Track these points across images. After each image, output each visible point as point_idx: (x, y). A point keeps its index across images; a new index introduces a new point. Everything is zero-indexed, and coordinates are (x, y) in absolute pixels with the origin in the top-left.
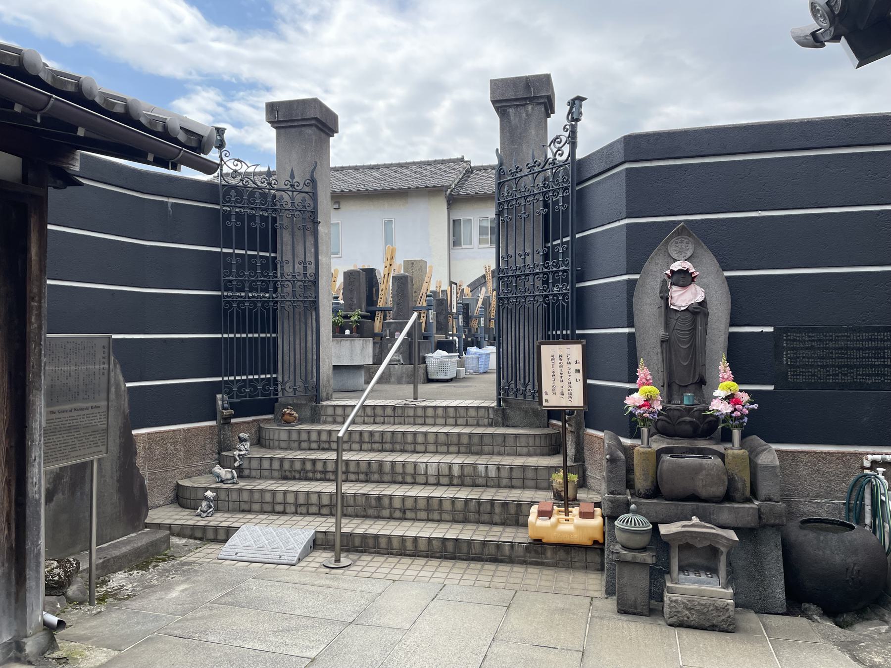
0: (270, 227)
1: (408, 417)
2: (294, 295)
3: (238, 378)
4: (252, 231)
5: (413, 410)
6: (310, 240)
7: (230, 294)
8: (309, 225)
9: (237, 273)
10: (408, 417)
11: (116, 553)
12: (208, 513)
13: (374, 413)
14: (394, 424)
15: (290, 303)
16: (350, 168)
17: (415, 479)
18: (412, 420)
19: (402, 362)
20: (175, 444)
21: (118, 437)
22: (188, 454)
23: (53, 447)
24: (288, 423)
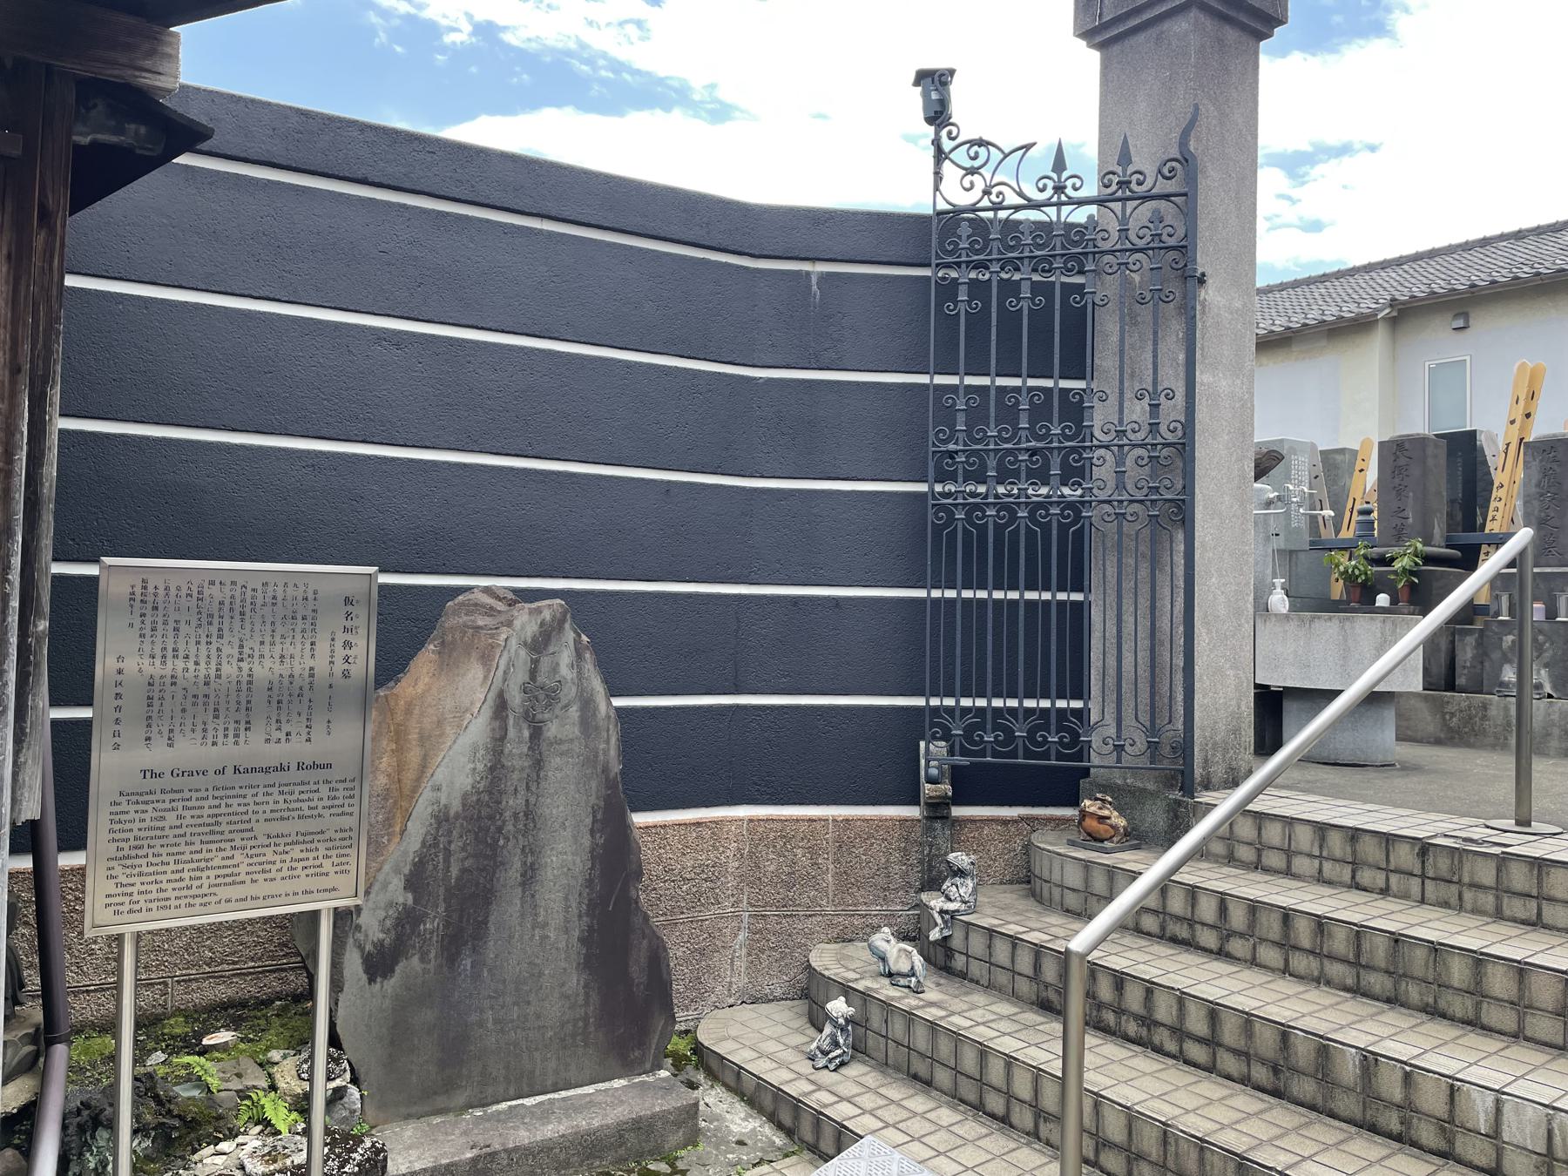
0: (1057, 306)
1: (1475, 886)
2: (1120, 486)
3: (966, 702)
4: (1010, 321)
5: (1492, 865)
6: (1174, 332)
7: (951, 488)
8: (1174, 287)
9: (968, 432)
10: (1475, 886)
11: (523, 1136)
12: (830, 1061)
13: (1354, 852)
14: (1423, 901)
15: (1107, 508)
16: (1503, 237)
17: (1451, 1142)
18: (1488, 900)
19: (1548, 689)
20: (813, 851)
21: (585, 831)
22: (845, 881)
23: (151, 869)
24: (1094, 839)
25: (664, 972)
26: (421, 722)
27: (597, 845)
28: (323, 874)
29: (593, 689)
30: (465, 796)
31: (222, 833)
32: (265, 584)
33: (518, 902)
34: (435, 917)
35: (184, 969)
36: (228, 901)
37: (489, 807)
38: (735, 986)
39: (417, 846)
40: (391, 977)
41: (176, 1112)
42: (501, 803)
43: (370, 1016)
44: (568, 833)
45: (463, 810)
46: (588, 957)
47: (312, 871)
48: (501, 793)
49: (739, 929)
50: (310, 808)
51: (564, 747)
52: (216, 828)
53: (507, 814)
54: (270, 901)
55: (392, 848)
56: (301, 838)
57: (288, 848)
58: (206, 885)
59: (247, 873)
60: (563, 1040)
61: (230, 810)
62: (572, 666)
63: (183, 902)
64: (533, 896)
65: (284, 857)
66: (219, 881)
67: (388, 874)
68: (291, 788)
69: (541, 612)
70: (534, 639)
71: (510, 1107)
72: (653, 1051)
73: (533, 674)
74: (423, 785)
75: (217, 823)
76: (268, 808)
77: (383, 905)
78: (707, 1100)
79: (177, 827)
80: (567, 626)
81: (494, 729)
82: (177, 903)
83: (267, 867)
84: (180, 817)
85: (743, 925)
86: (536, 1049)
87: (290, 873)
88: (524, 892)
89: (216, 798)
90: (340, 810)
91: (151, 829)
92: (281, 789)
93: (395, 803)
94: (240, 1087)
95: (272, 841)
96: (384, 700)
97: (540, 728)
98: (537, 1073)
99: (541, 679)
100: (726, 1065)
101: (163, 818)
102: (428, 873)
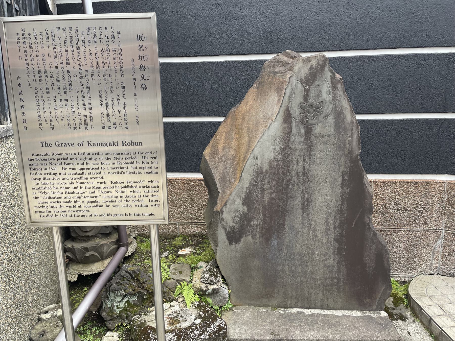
21: (338, 185)
23: (54, 195)
25: (385, 262)
26: (248, 124)
27: (345, 193)
28: (144, 205)
29: (342, 106)
30: (270, 162)
31: (87, 179)
32: (88, 28)
33: (300, 217)
34: (258, 219)
35: (182, 220)
36: (96, 215)
37: (283, 168)
38: (434, 266)
39: (248, 185)
40: (239, 243)
41: (146, 288)
42: (290, 167)
43: (231, 259)
44: (328, 185)
45: (270, 169)
46: (339, 249)
47: (138, 203)
48: (289, 162)
49: (438, 238)
50: (133, 168)
51: (325, 139)
52: (84, 176)
53: (293, 173)
54: (117, 218)
55: (236, 184)
56: (130, 185)
57: (123, 190)
58: (83, 206)
59: (103, 202)
60: (326, 286)
61: (89, 166)
62: (330, 93)
63: (73, 214)
64: (308, 215)
65: (122, 194)
66: (89, 204)
67: (234, 197)
68: (121, 155)
69: (310, 61)
70: (306, 77)
71: (298, 312)
72: (377, 301)
73: (306, 97)
74: (249, 156)
75: (83, 173)
76: (109, 166)
77: (233, 210)
78: (409, 330)
79: (64, 174)
80: (326, 69)
81: (284, 128)
82: (70, 214)
83: (114, 199)
84: (63, 169)
85: (441, 237)
86: (312, 288)
87: (126, 203)
88: (303, 212)
89: (81, 159)
90: (150, 170)
91: (50, 174)
92: (115, 156)
93: (237, 163)
94: (179, 279)
95: (114, 185)
96: (234, 113)
97: (311, 128)
98: (312, 299)
99: (311, 101)
100: (423, 313)
101: (55, 169)
102: (254, 198)
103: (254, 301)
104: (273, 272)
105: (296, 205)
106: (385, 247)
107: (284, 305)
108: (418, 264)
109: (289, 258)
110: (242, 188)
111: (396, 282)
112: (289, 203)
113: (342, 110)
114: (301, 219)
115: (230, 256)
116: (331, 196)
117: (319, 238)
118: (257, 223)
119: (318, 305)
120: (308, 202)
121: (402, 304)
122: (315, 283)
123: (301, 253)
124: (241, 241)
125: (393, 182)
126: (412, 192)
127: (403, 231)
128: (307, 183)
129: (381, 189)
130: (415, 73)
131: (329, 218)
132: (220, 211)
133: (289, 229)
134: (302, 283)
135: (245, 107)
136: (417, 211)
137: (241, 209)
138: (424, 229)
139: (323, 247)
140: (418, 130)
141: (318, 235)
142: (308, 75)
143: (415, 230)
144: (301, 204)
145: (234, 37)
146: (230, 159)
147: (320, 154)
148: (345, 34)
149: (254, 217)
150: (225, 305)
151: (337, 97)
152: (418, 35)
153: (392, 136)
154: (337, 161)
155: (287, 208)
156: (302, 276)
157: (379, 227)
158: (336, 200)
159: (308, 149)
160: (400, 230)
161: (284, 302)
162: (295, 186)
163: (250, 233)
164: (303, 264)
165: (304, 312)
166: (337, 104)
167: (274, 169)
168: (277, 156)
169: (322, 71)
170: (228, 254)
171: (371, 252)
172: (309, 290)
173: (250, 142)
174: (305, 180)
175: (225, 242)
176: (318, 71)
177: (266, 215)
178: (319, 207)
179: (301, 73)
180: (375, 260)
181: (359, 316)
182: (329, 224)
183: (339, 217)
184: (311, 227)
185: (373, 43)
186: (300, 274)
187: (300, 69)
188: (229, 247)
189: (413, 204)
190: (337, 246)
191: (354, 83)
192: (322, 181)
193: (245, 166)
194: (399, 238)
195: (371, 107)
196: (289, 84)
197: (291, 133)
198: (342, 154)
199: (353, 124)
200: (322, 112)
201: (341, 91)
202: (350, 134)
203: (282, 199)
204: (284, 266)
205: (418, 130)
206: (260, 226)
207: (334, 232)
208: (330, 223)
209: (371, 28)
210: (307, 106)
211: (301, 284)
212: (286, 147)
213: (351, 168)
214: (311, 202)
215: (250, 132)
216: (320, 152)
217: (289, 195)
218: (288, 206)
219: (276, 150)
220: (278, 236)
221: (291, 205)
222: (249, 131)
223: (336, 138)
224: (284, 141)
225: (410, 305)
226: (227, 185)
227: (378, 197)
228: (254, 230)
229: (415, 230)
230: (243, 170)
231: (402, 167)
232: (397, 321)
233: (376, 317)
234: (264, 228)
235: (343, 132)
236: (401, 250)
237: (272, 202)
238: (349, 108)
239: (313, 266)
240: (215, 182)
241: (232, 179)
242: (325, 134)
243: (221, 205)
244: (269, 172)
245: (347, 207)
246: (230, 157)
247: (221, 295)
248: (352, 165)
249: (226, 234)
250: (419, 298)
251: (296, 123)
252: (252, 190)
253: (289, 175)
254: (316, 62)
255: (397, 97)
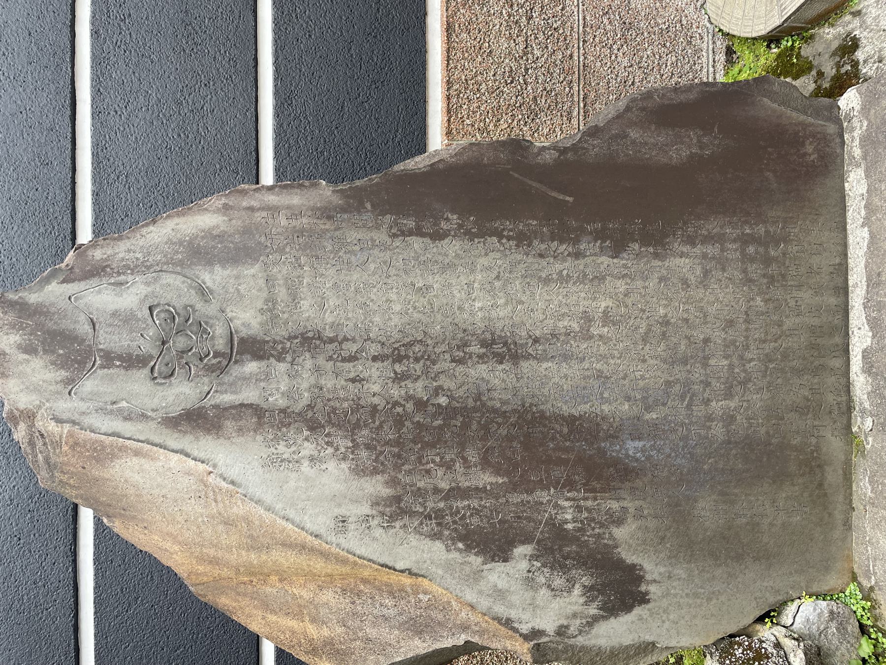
21: (435, 249)
25: (683, 97)
27: (460, 226)
29: (170, 242)
30: (359, 471)
33: (545, 365)
34: (556, 506)
37: (381, 426)
39: (438, 545)
40: (642, 569)
42: (376, 406)
43: (696, 595)
44: (436, 281)
45: (383, 472)
46: (647, 239)
51: (282, 293)
53: (396, 392)
60: (772, 280)
64: (536, 341)
70: (63, 363)
72: (810, 120)
74: (334, 550)
77: (529, 594)
80: (33, 298)
88: (528, 357)
97: (242, 341)
98: (816, 322)
99: (147, 346)
103: (836, 512)
104: (734, 452)
105: (504, 381)
106: (633, 100)
107: (843, 413)
108: (676, 16)
109: (682, 398)
110: (448, 567)
111: (730, 75)
112: (498, 405)
113: (181, 243)
114: (550, 364)
115: (687, 600)
116: (472, 271)
117: (611, 304)
118: (571, 511)
119: (835, 303)
120: (494, 342)
121: (799, 52)
122: (763, 314)
123: (665, 361)
124: (635, 562)
125: (448, 89)
126: (475, 39)
127: (585, 58)
128: (430, 348)
129: (468, 119)
130: (143, 36)
131: (544, 276)
132: (532, 643)
133: (586, 403)
134: (767, 355)
135: (174, 556)
136: (528, 23)
137: (524, 565)
138: (578, 5)
139: (642, 290)
140: (304, 25)
141: (603, 306)
142: (53, 358)
143: (581, 28)
144: (501, 363)
145: (22, 541)
146: (353, 603)
147: (332, 307)
148: (27, 225)
149: (551, 523)
150: (855, 612)
151: (137, 259)
152: (38, 30)
153: (320, 94)
154: (356, 255)
155: (515, 411)
156: (741, 358)
157: (575, 122)
158: (486, 254)
159: (316, 347)
160: (582, 68)
161: (830, 412)
162: (440, 387)
163: (604, 533)
164: (700, 354)
165: (864, 351)
166: (159, 258)
167: (382, 458)
168: (337, 449)
169: (41, 313)
170: (680, 607)
171: (652, 140)
172: (788, 333)
173: (287, 545)
174: (419, 355)
175: (641, 618)
176: (39, 326)
177: (541, 480)
178: (510, 308)
179: (44, 381)
180: (677, 129)
181: (867, 177)
182: (565, 272)
183: (542, 241)
184: (578, 329)
185: (56, 149)
186: (735, 360)
187: (27, 388)
188: (657, 604)
189: (510, 33)
190: (636, 246)
191: (168, 198)
192: (422, 299)
193: (370, 560)
194: (606, 69)
195: (238, 151)
196: (78, 424)
197: (258, 405)
198: (332, 238)
199: (231, 208)
200: (185, 307)
201: (115, 247)
202: (264, 214)
203: (485, 428)
204: (711, 415)
205: (304, 25)
206: (579, 500)
207: (592, 258)
208: (562, 271)
209: (14, 156)
210: (164, 358)
211: (768, 359)
212: (306, 421)
213: (381, 209)
214: (493, 334)
215: (255, 544)
216: (326, 310)
217: (470, 403)
218: (510, 408)
219: (316, 453)
220: (613, 436)
221: (504, 397)
222: (252, 547)
223: (278, 258)
224: (284, 429)
225: (802, 28)
226: (440, 617)
227: (491, 127)
228: (593, 520)
229: (581, 28)
230: (387, 566)
231: (408, 66)
232: (862, 63)
233: (865, 123)
234: (584, 485)
235: (257, 236)
236: (639, 63)
237: (494, 460)
238: (176, 220)
239: (706, 323)
240: (433, 651)
241: (421, 601)
242: (265, 295)
243: (512, 637)
244: (393, 474)
245: (507, 219)
246: (344, 603)
247: (822, 628)
248: (368, 206)
249: (612, 615)
250: (782, 5)
251: (222, 393)
252: (456, 530)
253: (404, 406)
254: (7, 334)
255: (211, 83)
